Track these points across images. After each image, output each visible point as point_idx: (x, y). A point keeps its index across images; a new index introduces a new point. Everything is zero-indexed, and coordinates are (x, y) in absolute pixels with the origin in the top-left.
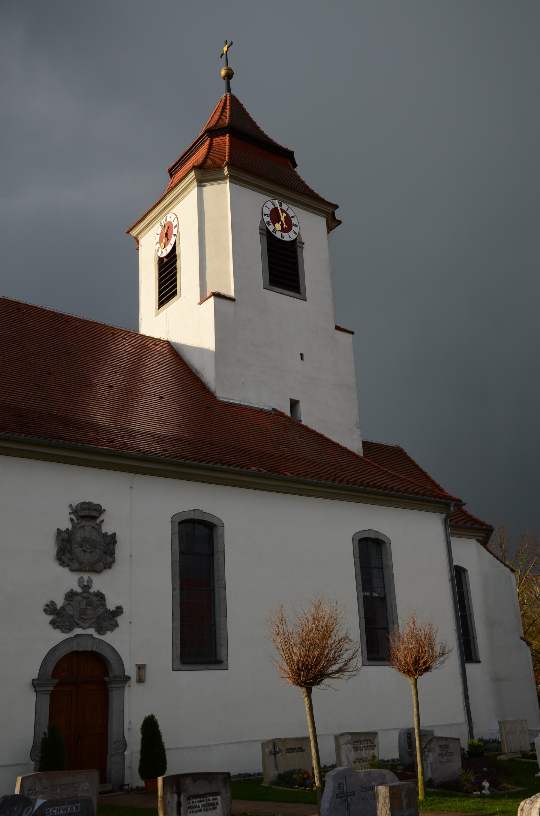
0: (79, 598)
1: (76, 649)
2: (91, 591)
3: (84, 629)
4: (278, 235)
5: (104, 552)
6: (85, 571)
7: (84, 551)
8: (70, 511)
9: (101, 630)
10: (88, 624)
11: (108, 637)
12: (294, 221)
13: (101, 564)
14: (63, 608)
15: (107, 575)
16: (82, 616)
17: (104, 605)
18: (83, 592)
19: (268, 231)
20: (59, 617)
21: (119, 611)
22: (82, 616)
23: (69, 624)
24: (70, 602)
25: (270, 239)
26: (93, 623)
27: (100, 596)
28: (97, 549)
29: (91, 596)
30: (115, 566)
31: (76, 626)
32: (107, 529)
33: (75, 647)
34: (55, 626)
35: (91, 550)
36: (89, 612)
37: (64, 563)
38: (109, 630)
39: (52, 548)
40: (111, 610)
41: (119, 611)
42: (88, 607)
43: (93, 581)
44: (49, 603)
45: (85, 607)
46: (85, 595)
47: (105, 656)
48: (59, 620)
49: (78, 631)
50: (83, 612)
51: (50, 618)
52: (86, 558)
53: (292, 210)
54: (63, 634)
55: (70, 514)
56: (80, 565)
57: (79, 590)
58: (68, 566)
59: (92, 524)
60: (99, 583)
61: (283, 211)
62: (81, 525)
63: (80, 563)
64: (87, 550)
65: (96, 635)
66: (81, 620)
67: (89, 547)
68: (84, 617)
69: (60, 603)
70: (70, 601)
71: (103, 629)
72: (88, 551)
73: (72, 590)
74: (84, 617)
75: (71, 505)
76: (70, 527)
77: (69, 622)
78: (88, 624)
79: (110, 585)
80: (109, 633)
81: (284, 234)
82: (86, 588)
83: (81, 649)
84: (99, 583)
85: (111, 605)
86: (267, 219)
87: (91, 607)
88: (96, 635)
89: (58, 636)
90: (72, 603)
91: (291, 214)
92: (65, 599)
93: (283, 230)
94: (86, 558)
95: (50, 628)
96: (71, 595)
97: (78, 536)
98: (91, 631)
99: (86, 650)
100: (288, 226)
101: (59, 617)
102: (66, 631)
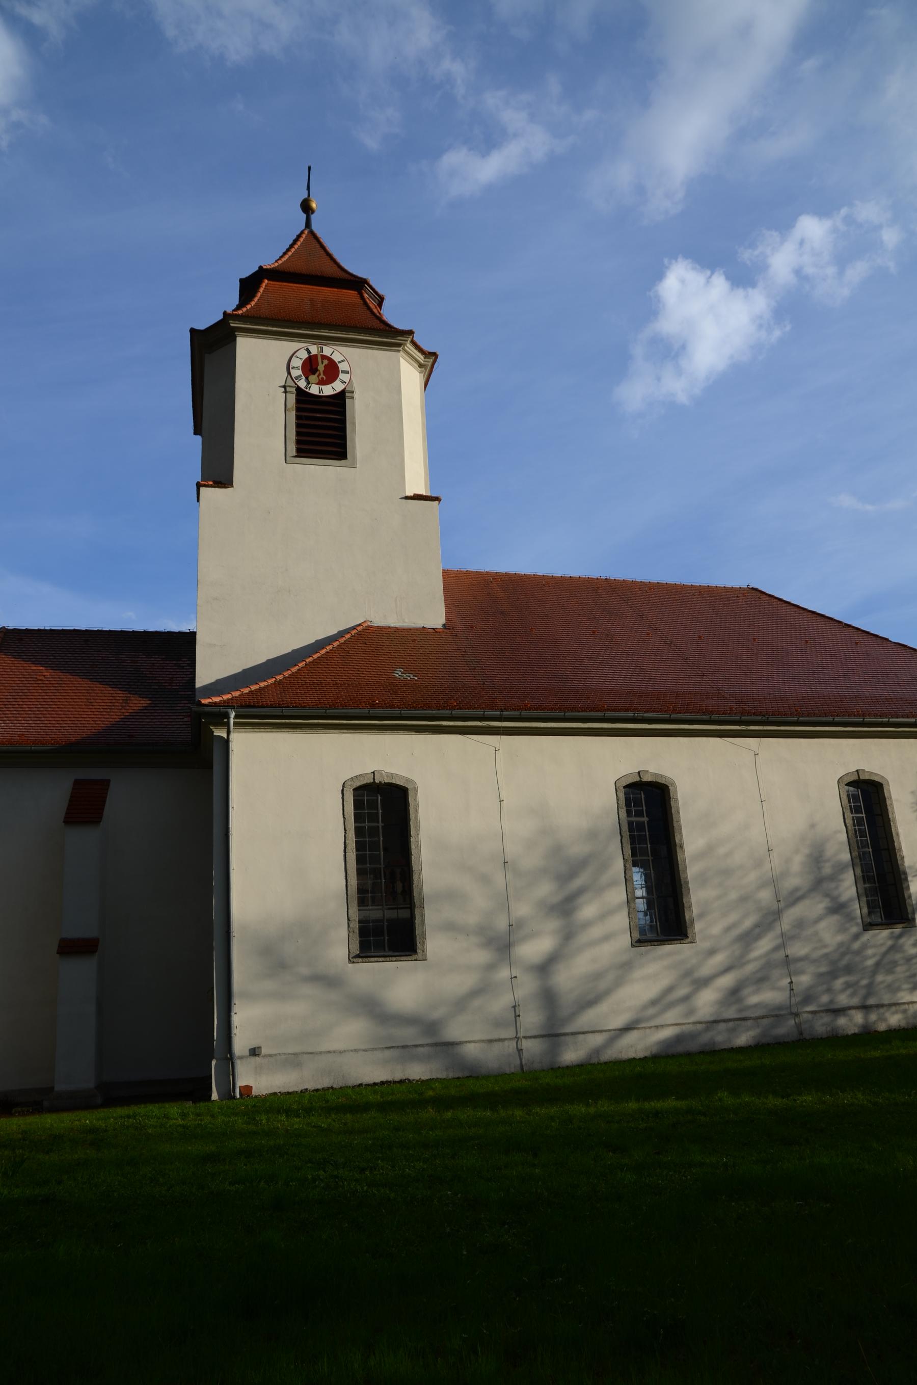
4: (314, 390)
12: (342, 366)
19: (299, 389)
25: (302, 396)
53: (336, 352)
61: (324, 357)
81: (323, 387)
86: (296, 373)
91: (336, 357)
93: (321, 382)
100: (332, 371)
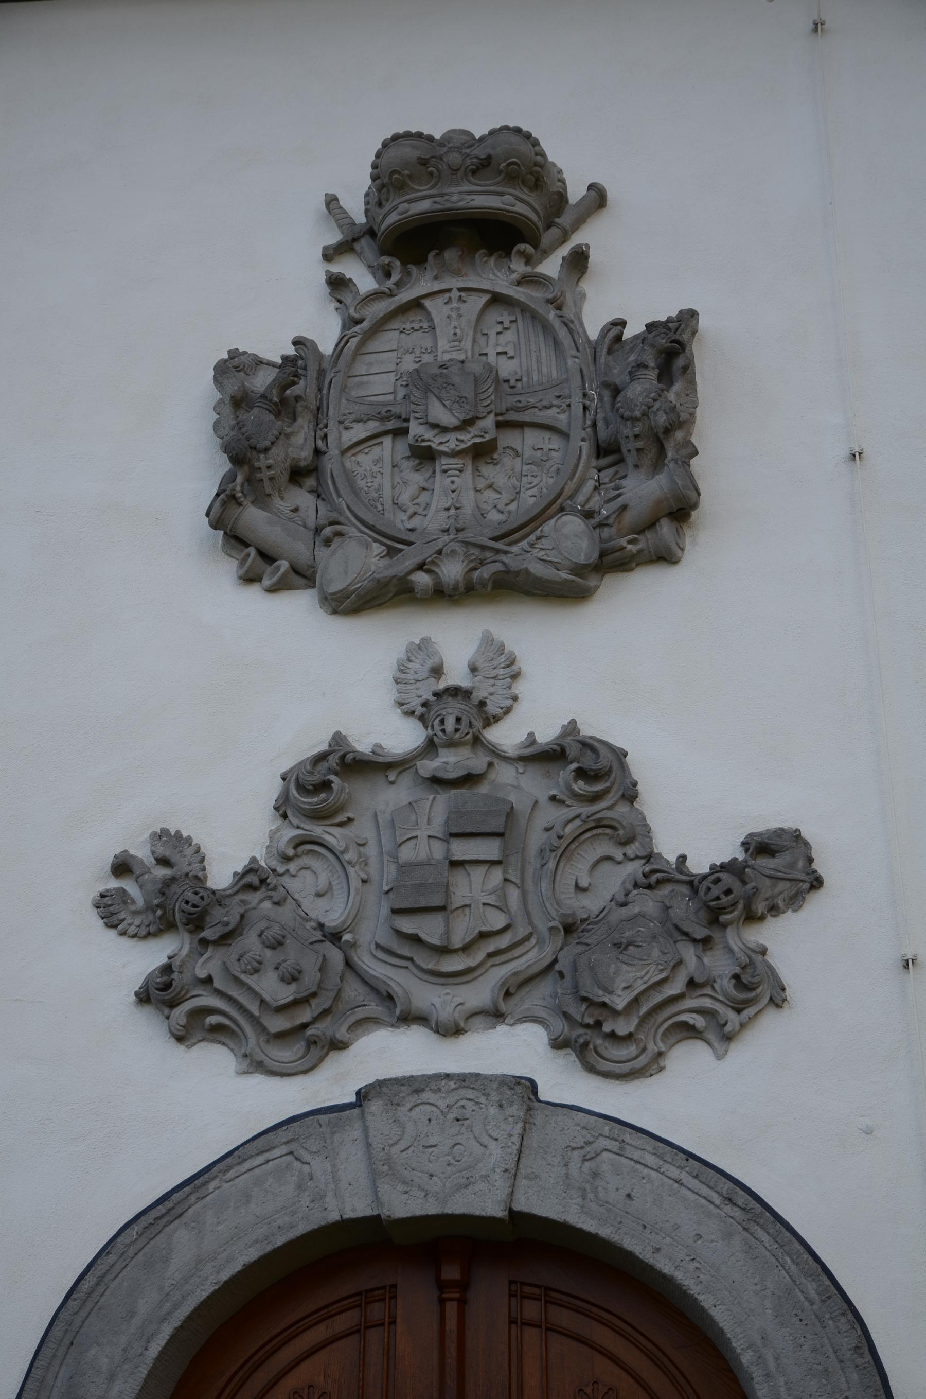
0: (390, 797)
1: (358, 1207)
2: (507, 736)
3: (451, 1030)
5: (601, 450)
6: (444, 596)
7: (424, 456)
8: (334, 237)
9: (588, 1036)
10: (479, 993)
11: (690, 1098)
13: (572, 524)
14: (253, 879)
15: (635, 605)
16: (407, 925)
17: (633, 836)
18: (430, 747)
20: (209, 947)
21: (774, 870)
22: (407, 925)
23: (286, 994)
24: (317, 830)
26: (527, 981)
27: (589, 769)
28: (532, 438)
29: (505, 774)
30: (709, 547)
31: (374, 1008)
32: (623, 293)
33: (348, 1192)
34: (180, 1013)
35: (469, 438)
36: (470, 888)
37: (267, 557)
38: (689, 1031)
39: (194, 470)
40: (699, 865)
41: (777, 869)
42: (462, 850)
43: (525, 664)
44: (142, 852)
45: (438, 851)
46: (450, 761)
47: (665, 1266)
48: (209, 964)
49: (388, 1053)
50: (418, 899)
51: (147, 958)
52: (441, 503)
54: (258, 1081)
55: (329, 255)
56: (391, 552)
57: (401, 736)
58: (302, 576)
59: (498, 277)
60: (566, 671)
62: (405, 296)
63: (394, 544)
64: (435, 441)
65: (563, 1083)
66: (423, 951)
67: (446, 418)
68: (430, 929)
69: (234, 836)
70: (317, 816)
71: (622, 1027)
72: (451, 442)
73: (338, 739)
74: (430, 929)
75: (331, 201)
76: (326, 332)
77: (292, 978)
78: (479, 993)
79: (680, 694)
80: (690, 1061)
82: (456, 712)
83: (402, 1205)
84: (566, 671)
85: (694, 828)
87: (488, 849)
88: (563, 1083)
89: (217, 1101)
90: (334, 836)
92: (283, 809)
94: (441, 503)
95: (144, 1040)
96: (326, 783)
97: (380, 377)
98: (518, 1049)
99: (458, 1205)
101: (209, 947)
102: (285, 1054)
